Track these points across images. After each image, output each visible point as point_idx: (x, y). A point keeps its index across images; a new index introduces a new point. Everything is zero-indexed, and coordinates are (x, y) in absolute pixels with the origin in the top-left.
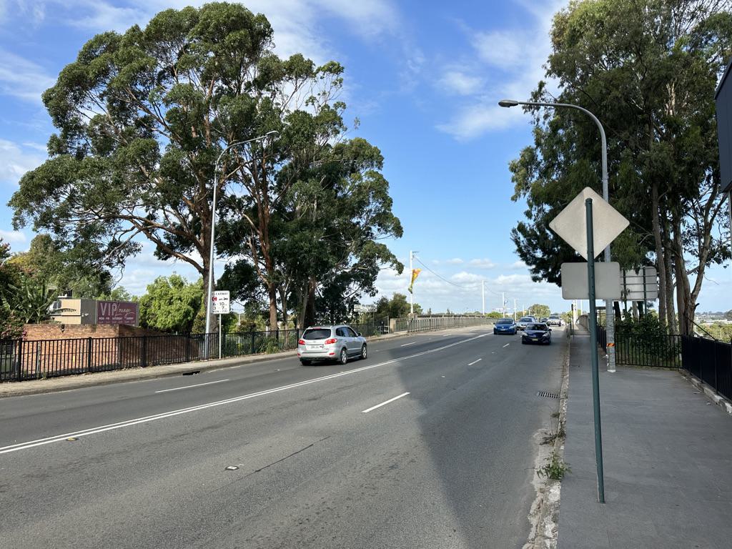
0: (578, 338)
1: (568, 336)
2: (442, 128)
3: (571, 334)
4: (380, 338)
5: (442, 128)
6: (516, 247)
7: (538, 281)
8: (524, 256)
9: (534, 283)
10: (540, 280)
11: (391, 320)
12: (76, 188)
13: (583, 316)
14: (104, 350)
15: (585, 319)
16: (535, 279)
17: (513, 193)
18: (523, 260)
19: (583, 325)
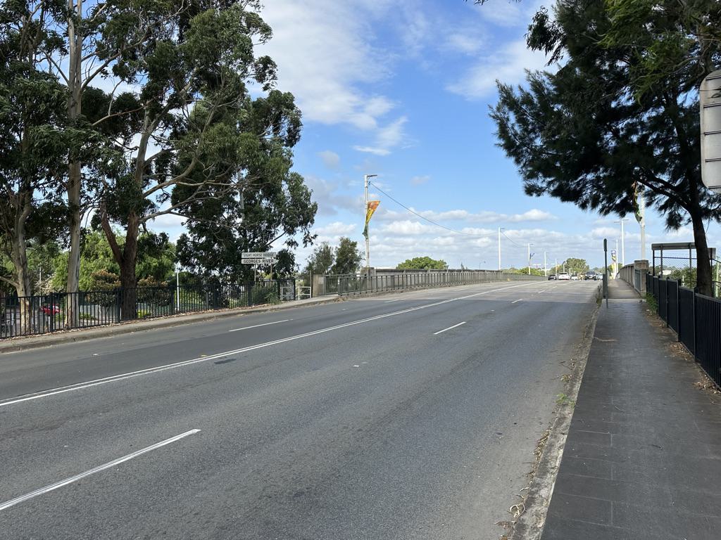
0: (616, 306)
1: (599, 301)
2: (453, 89)
3: (604, 297)
4: (276, 306)
5: (453, 89)
6: (496, 129)
7: (535, 195)
8: (512, 147)
9: (528, 197)
10: (539, 191)
11: (314, 276)
12: (169, 172)
13: (626, 267)
14: (409, 284)
15: (627, 273)
16: (530, 190)
17: (500, 82)
18: (510, 154)
19: (625, 280)
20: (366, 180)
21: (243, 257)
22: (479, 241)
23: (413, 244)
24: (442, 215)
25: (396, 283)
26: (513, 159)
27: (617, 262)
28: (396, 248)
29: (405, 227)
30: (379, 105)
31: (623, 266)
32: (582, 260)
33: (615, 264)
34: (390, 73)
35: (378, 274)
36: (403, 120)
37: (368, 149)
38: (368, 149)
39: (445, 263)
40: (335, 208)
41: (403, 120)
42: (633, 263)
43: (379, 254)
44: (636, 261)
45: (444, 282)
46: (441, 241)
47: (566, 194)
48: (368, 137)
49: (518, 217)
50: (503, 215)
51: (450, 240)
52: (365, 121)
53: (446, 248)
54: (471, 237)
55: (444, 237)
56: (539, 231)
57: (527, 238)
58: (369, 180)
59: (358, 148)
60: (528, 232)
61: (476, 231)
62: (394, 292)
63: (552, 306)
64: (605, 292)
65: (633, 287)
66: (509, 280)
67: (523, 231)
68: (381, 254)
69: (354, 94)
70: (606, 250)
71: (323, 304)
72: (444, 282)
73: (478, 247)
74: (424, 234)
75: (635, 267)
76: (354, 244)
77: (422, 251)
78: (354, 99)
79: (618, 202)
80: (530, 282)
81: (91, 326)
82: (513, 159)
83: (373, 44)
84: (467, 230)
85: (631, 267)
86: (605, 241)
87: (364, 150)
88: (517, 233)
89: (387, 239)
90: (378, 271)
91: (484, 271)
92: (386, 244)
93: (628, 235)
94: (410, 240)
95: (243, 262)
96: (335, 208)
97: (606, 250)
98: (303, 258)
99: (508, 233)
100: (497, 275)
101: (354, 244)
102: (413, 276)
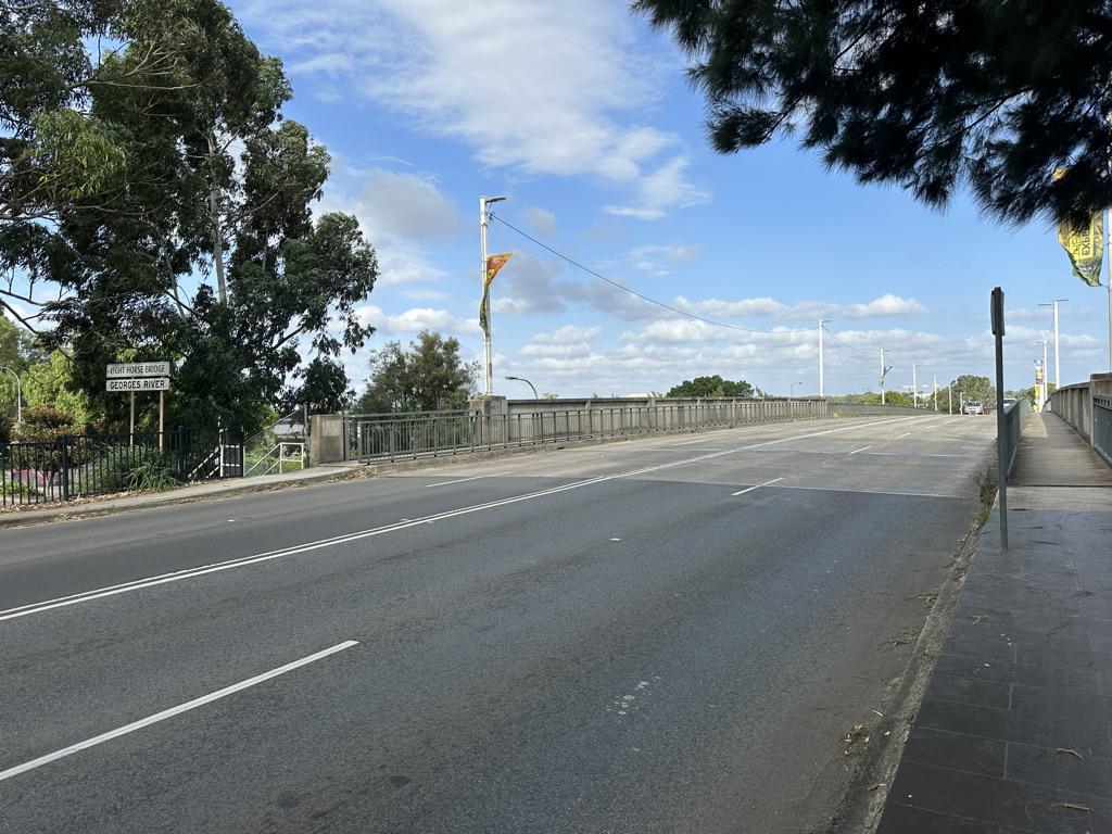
9: (731, 157)
13: (1064, 391)
15: (1070, 406)
20: (483, 208)
21: (109, 375)
22: (798, 350)
23: (692, 357)
24: (733, 307)
25: (687, 420)
26: (671, 29)
27: (1046, 381)
28: (665, 363)
29: (678, 329)
30: (644, 141)
31: (1058, 388)
32: (985, 378)
33: (1042, 386)
34: (658, 93)
35: (515, 411)
36: (680, 162)
37: (627, 212)
38: (627, 212)
39: (749, 386)
40: (560, 299)
41: (680, 162)
42: (1088, 380)
43: (498, 368)
44: (1095, 376)
45: (682, 424)
46: (738, 351)
47: (875, 151)
48: (625, 193)
49: (862, 308)
50: (835, 306)
51: (752, 348)
52: (619, 166)
53: (745, 362)
54: (784, 344)
55: (742, 344)
56: (898, 333)
57: (879, 343)
58: (490, 211)
59: (612, 210)
60: (880, 334)
61: (794, 335)
62: (535, 450)
63: (848, 504)
64: (1012, 457)
65: (1087, 438)
66: (836, 415)
67: (871, 333)
68: (644, 373)
69: (604, 127)
70: (998, 330)
71: (294, 488)
72: (682, 424)
73: (798, 359)
74: (711, 341)
75: (1092, 392)
76: (452, 346)
77: (707, 367)
78: (603, 134)
79: (1056, 172)
80: (875, 418)
81: (623, 430)
82: (671, 29)
83: (628, 49)
84: (779, 332)
85: (1082, 390)
86: (997, 295)
87: (619, 212)
88: (860, 336)
89: (650, 349)
90: (512, 404)
91: (785, 399)
92: (653, 356)
93: (1044, 335)
94: (687, 351)
95: (108, 389)
96: (560, 299)
97: (998, 330)
98: (359, 373)
99: (846, 336)
100: (812, 406)
101: (452, 346)
102: (667, 409)
